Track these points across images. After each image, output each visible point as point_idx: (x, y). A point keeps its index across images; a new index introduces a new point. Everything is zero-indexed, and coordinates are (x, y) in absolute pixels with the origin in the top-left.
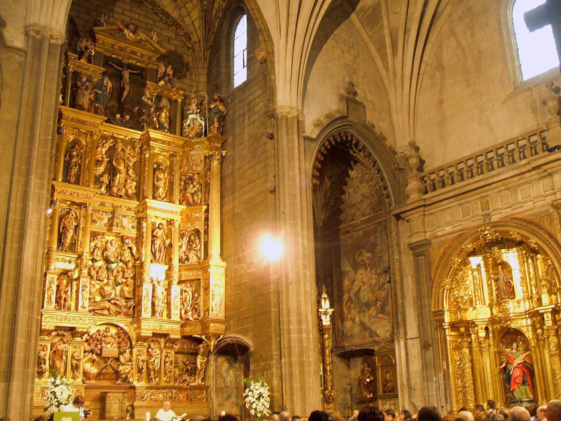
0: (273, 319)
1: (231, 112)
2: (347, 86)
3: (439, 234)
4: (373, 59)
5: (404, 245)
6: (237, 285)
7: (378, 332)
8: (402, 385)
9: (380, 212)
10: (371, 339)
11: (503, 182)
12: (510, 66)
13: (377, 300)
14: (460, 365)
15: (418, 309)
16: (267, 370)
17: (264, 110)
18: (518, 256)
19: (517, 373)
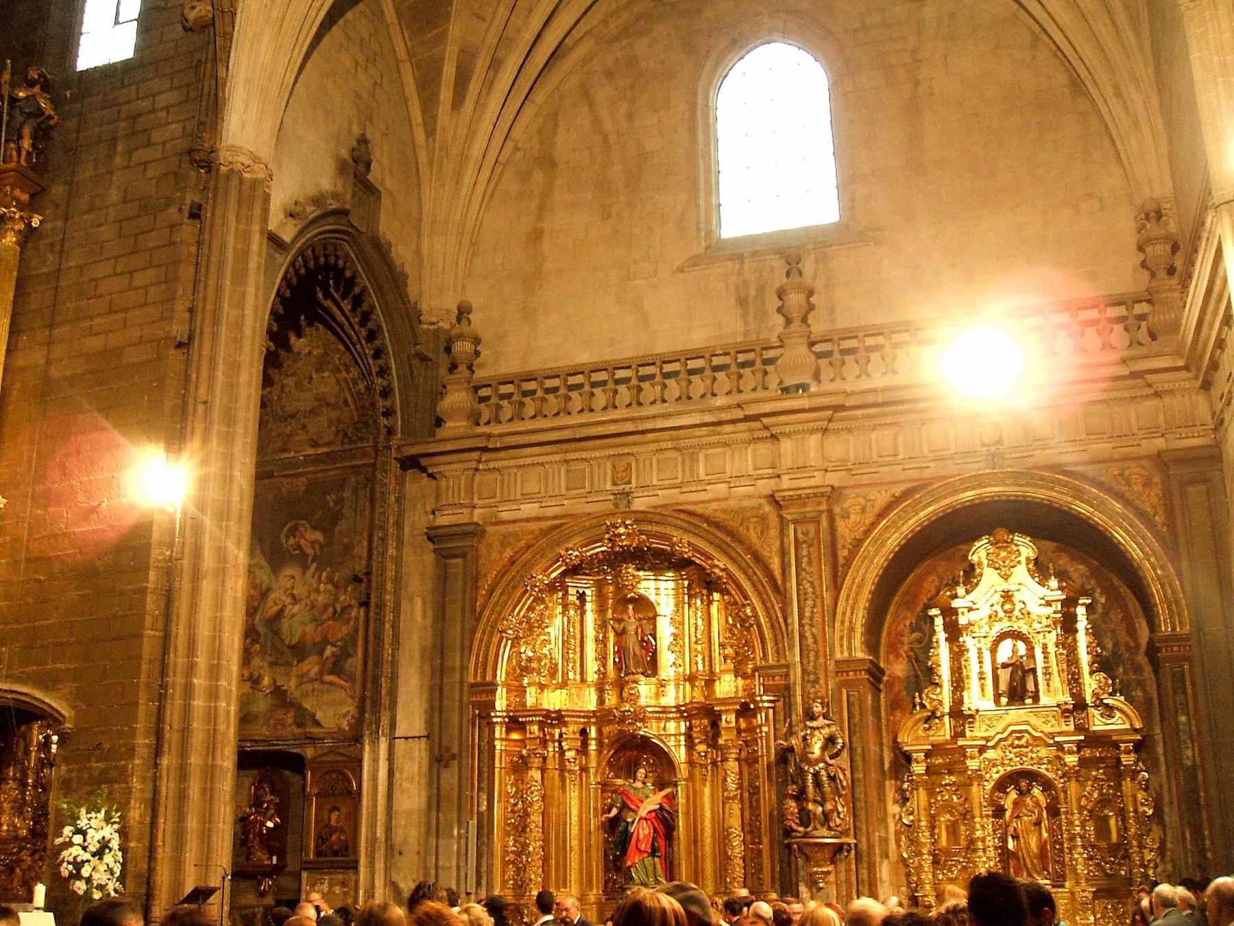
0: (146, 656)
1: (72, 124)
2: (355, 144)
3: (505, 516)
4: (406, 100)
5: (413, 527)
6: (36, 559)
7: (319, 716)
8: (373, 841)
9: (360, 444)
10: (298, 731)
11: (674, 433)
12: (702, 203)
13: (326, 641)
14: (516, 805)
15: (433, 674)
16: (111, 781)
17: (182, 144)
18: (676, 589)
19: (642, 831)
